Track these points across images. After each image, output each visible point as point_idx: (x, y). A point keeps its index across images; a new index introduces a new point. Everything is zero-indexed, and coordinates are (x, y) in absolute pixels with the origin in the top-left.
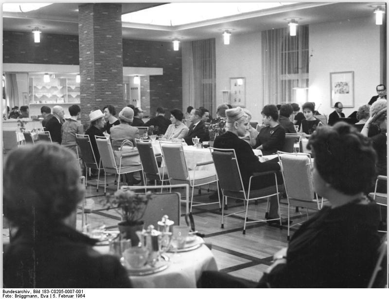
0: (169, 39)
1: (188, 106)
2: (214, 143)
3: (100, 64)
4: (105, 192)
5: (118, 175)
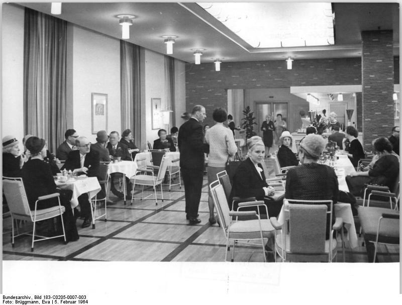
0: (211, 59)
1: (65, 132)
2: (58, 169)
3: (369, 87)
4: (33, 247)
5: (33, 223)
